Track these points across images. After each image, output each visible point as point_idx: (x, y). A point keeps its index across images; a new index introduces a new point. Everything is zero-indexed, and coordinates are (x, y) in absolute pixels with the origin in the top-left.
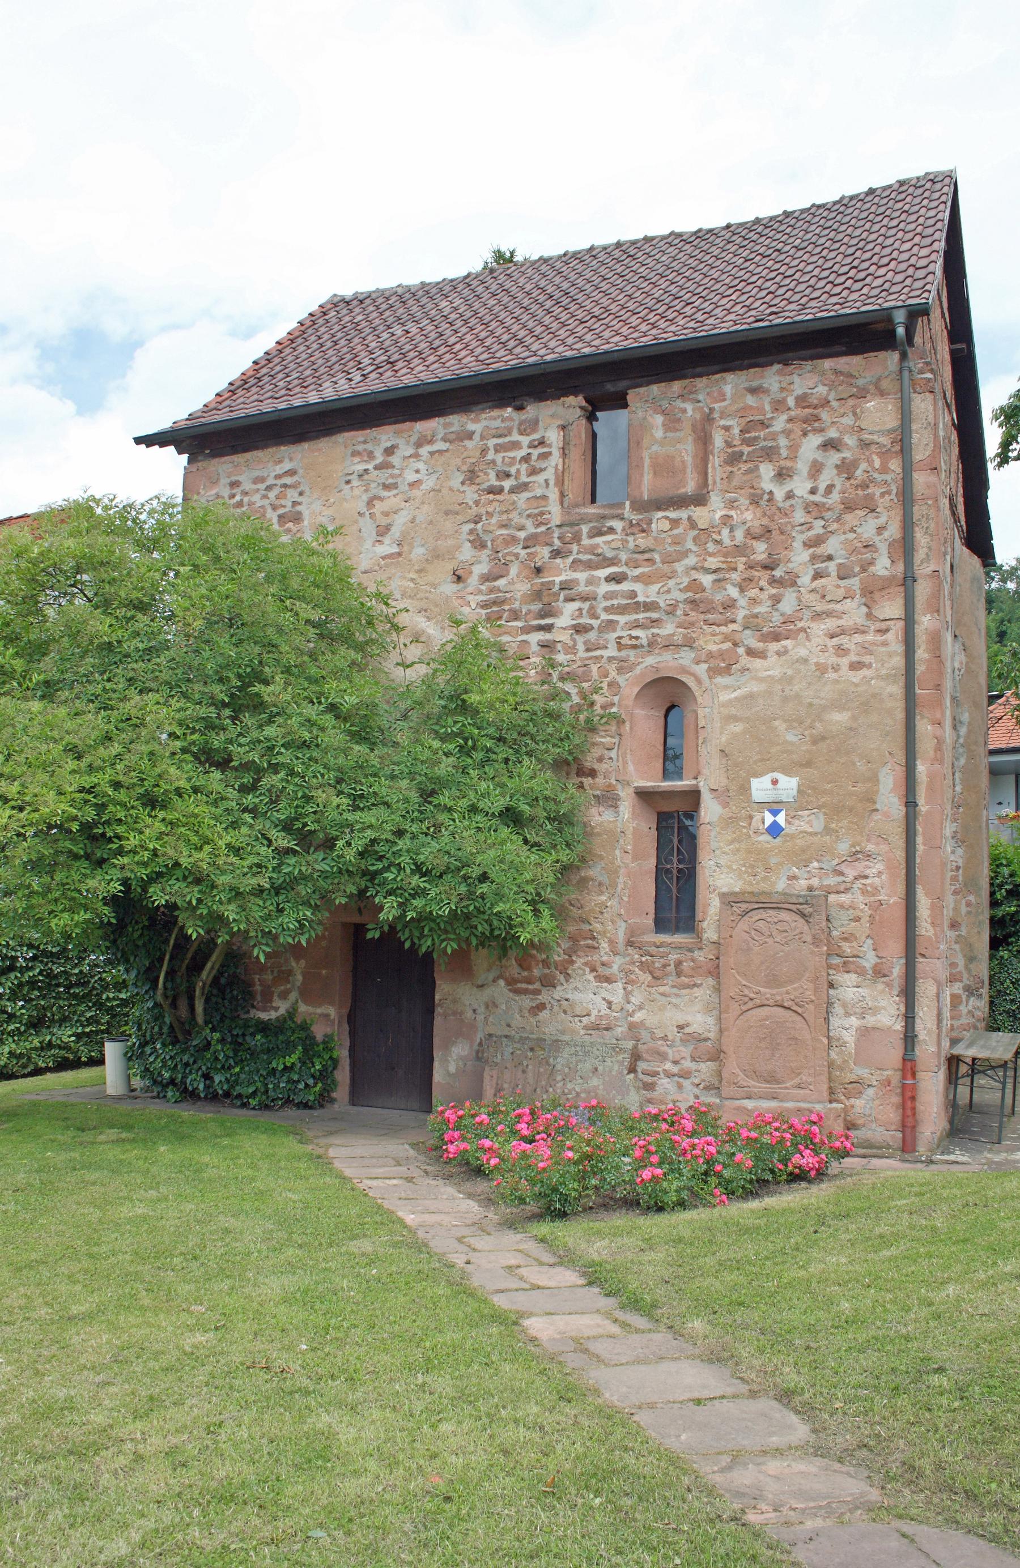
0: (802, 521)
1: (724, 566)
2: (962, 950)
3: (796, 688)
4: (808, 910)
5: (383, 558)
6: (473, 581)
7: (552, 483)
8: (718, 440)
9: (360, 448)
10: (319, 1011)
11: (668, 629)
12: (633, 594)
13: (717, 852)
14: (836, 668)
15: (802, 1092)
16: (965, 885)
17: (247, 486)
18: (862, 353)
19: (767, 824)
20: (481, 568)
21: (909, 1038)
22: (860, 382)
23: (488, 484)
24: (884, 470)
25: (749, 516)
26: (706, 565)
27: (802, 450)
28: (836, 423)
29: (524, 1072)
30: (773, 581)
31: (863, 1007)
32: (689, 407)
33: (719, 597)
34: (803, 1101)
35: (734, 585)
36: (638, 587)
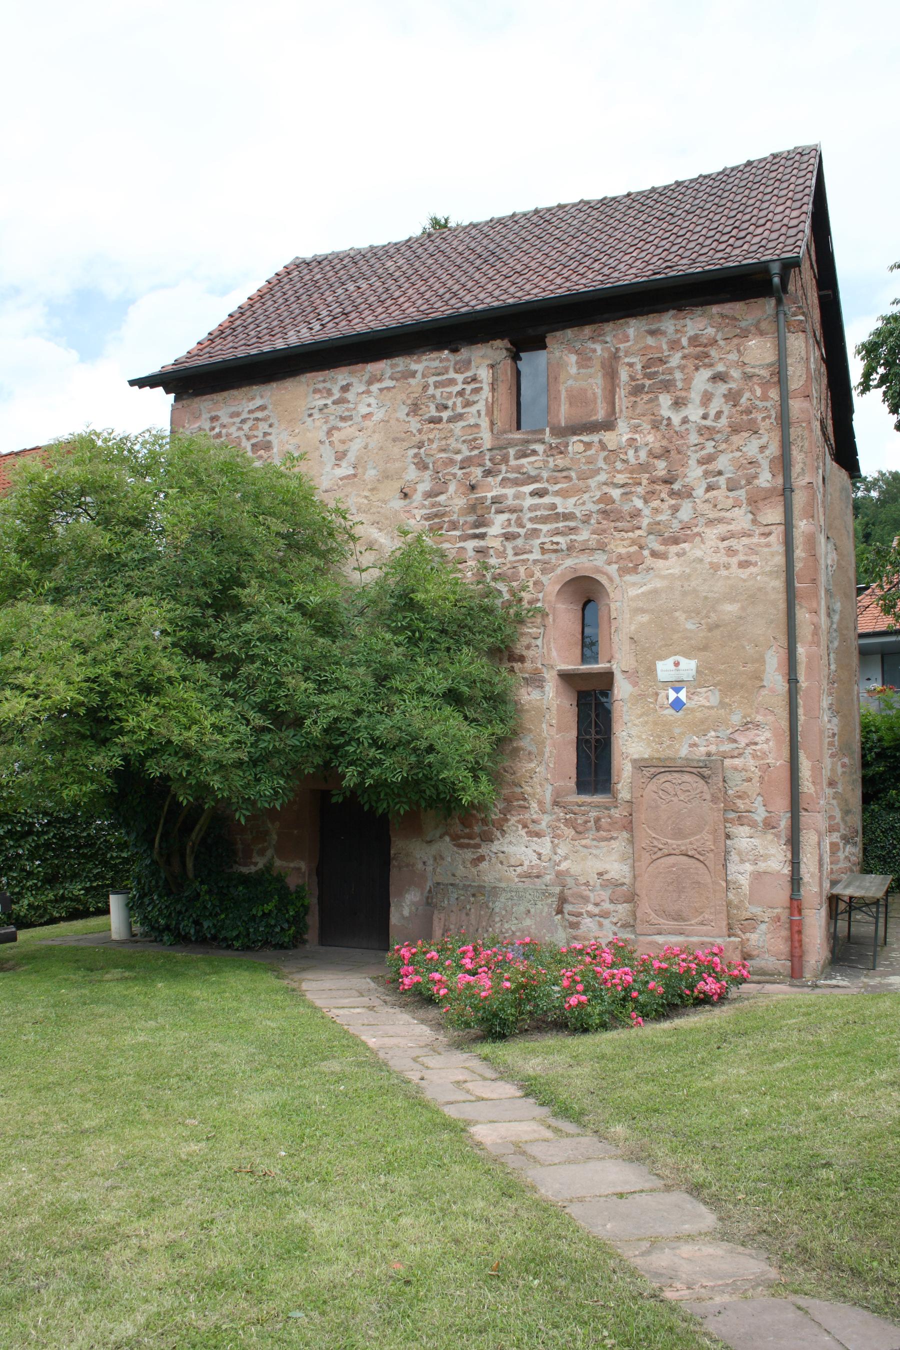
0: (696, 442)
1: (630, 481)
2: (839, 804)
4: (706, 772)
5: (341, 479)
6: (418, 497)
7: (483, 413)
8: (624, 375)
9: (320, 386)
10: (292, 865)
11: (584, 535)
12: (554, 507)
13: (629, 724)
14: (727, 567)
15: (704, 928)
16: (841, 749)
17: (225, 420)
20: (425, 486)
21: (795, 880)
22: (743, 324)
24: (765, 398)
26: (615, 481)
27: (694, 382)
29: (467, 914)
30: (672, 494)
31: (757, 856)
32: (598, 347)
33: (626, 508)
35: (640, 498)
36: (557, 500)
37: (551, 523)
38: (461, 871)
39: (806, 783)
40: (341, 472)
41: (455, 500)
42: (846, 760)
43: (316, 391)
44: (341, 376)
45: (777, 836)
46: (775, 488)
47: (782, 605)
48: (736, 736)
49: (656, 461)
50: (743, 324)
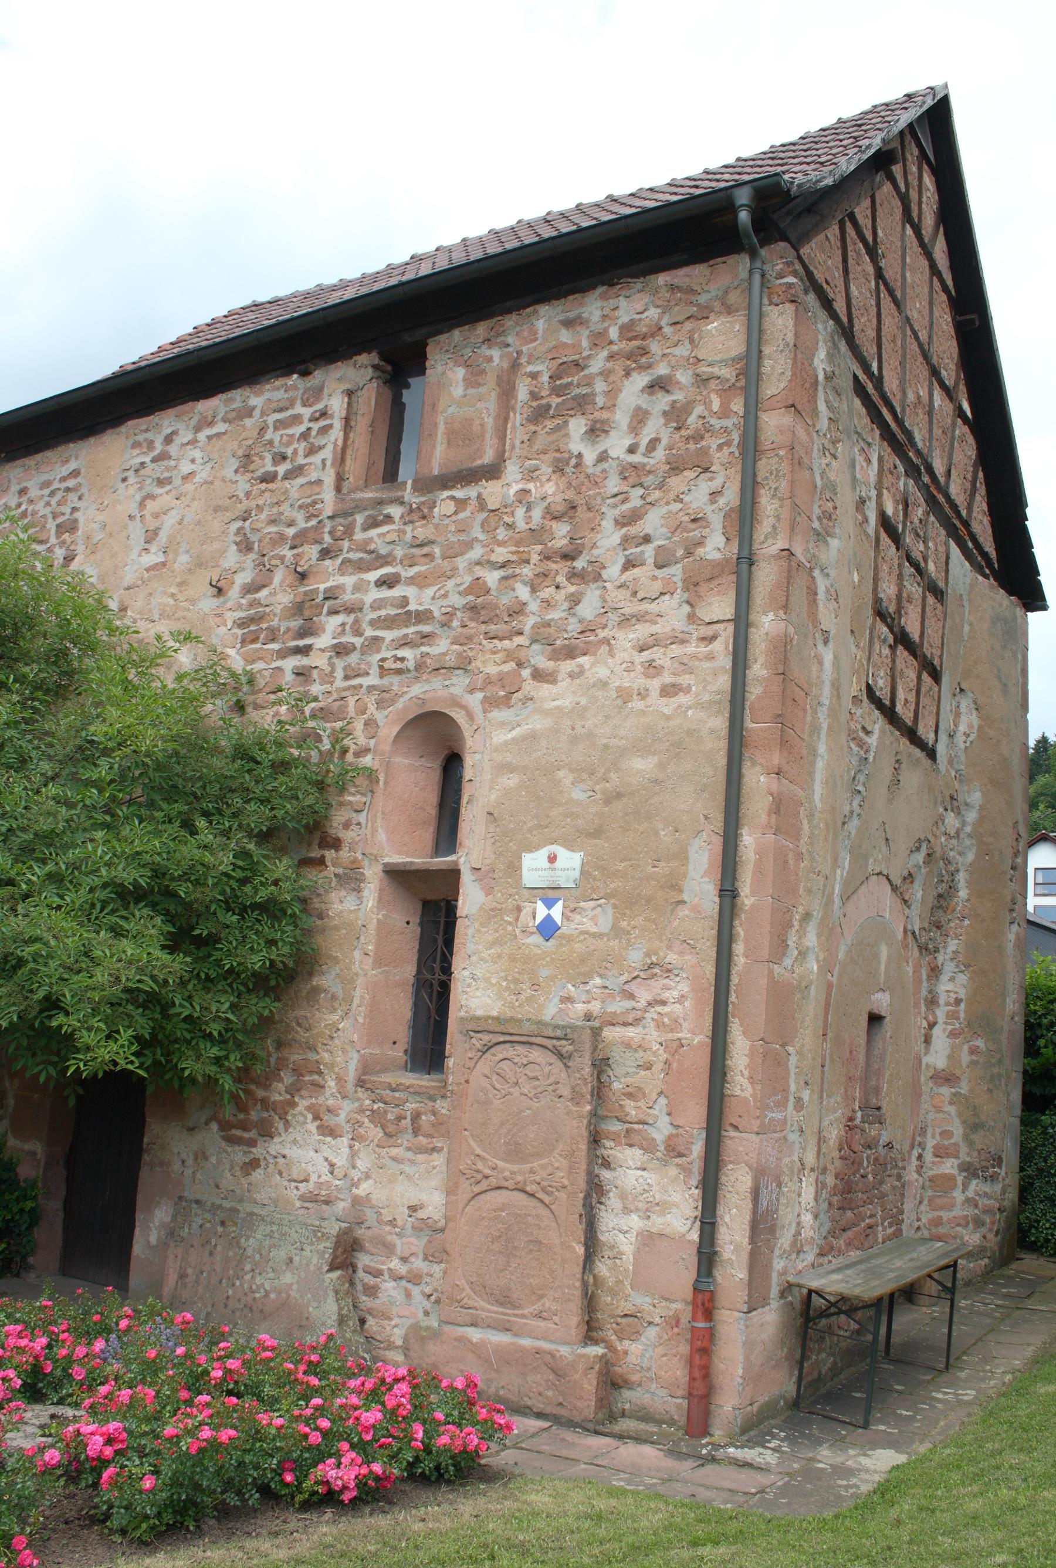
0: (615, 490)
1: (514, 558)
2: (960, 1115)
3: (589, 724)
4: (567, 1048)
5: (147, 570)
6: (234, 593)
7: (329, 463)
8: (522, 393)
9: (141, 438)
10: (27, 1147)
11: (441, 646)
12: (404, 601)
13: (474, 958)
14: (643, 695)
15: (543, 1324)
16: (969, 1025)
17: (34, 493)
18: (706, 260)
19: (539, 919)
20: (244, 578)
21: (707, 1256)
22: (703, 299)
23: (262, 470)
24: (725, 412)
25: (550, 489)
26: (493, 558)
27: (622, 395)
28: (668, 357)
29: (211, 1254)
30: (574, 576)
31: (650, 1203)
32: (496, 354)
33: (505, 600)
34: (545, 1338)
35: (525, 584)
36: (410, 592)
37: (399, 627)
38: (227, 1181)
39: (739, 1078)
40: (149, 560)
41: (279, 596)
42: (980, 1043)
43: (136, 445)
44: (167, 421)
45: (686, 1170)
46: (727, 560)
47: (722, 761)
48: (633, 987)
49: (554, 524)
50: (703, 299)
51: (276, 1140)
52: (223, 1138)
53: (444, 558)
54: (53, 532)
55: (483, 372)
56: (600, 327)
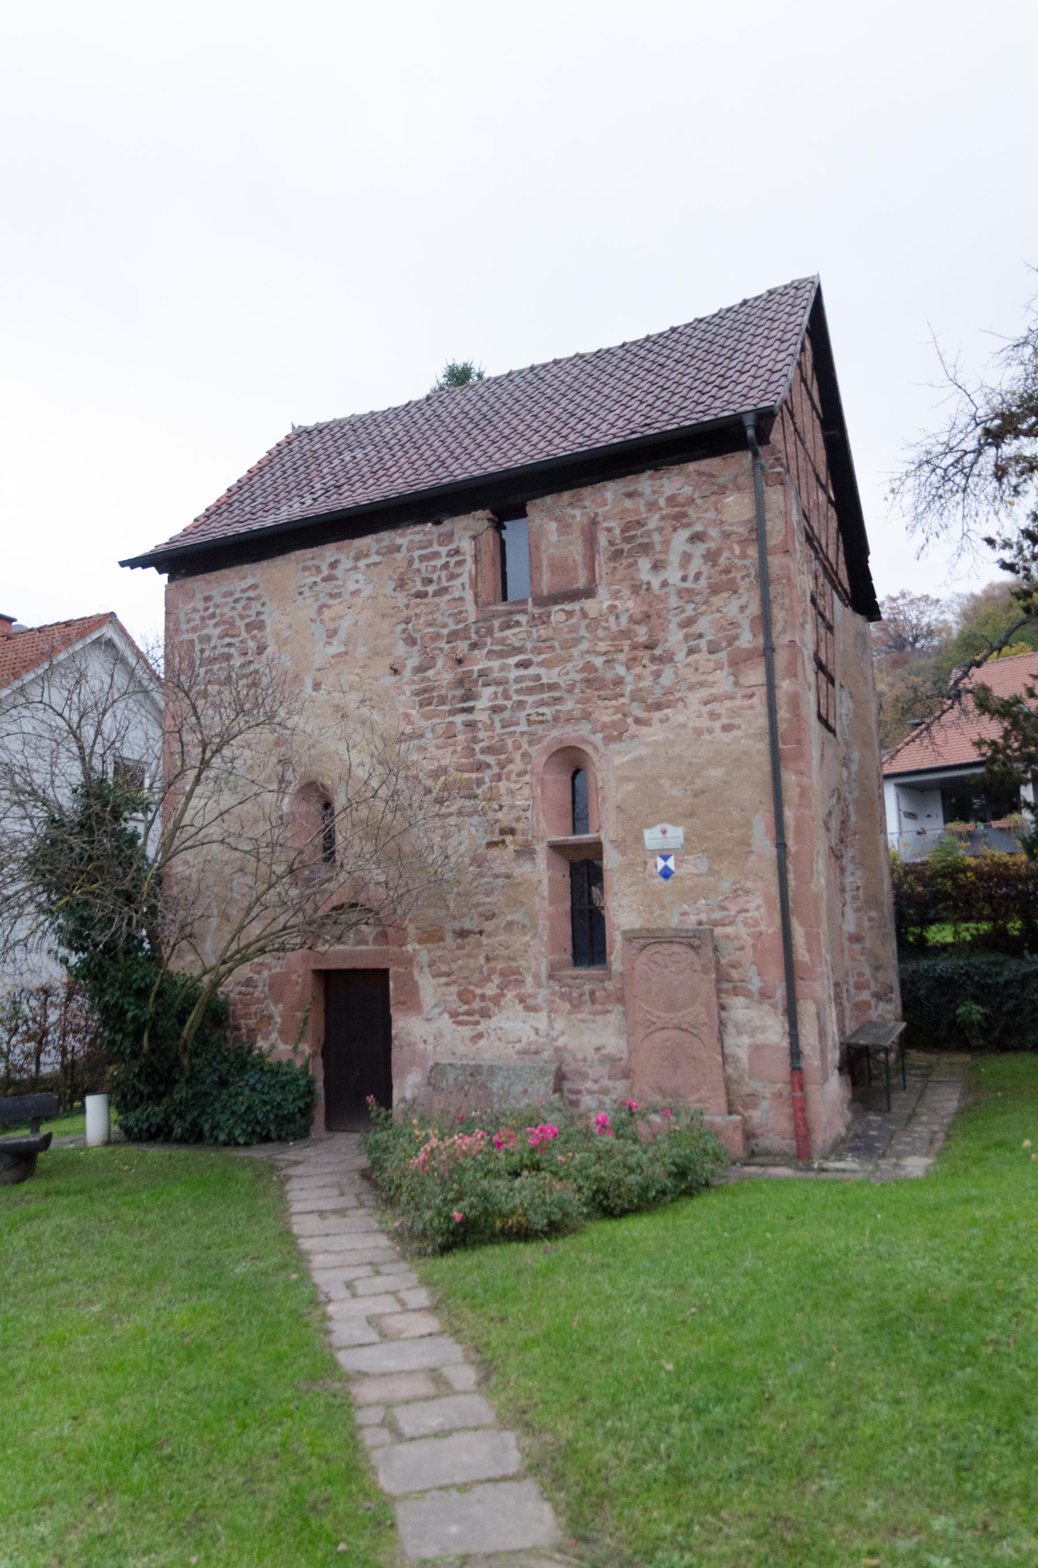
5: (333, 657)
6: (407, 673)
7: (467, 586)
8: (603, 540)
9: (309, 563)
11: (569, 705)
14: (710, 731)
17: (218, 599)
20: (413, 662)
22: (721, 480)
24: (744, 556)
25: (630, 605)
26: (597, 649)
28: (701, 518)
30: (653, 659)
31: (757, 1027)
32: (577, 513)
33: (610, 675)
36: (541, 671)
39: (800, 951)
41: (443, 675)
43: (305, 569)
45: (774, 1006)
46: (756, 648)
47: (767, 768)
48: (726, 904)
49: (637, 627)
51: (494, 1019)
52: (455, 1022)
53: (562, 648)
54: (243, 628)
55: (569, 526)
56: (652, 498)
